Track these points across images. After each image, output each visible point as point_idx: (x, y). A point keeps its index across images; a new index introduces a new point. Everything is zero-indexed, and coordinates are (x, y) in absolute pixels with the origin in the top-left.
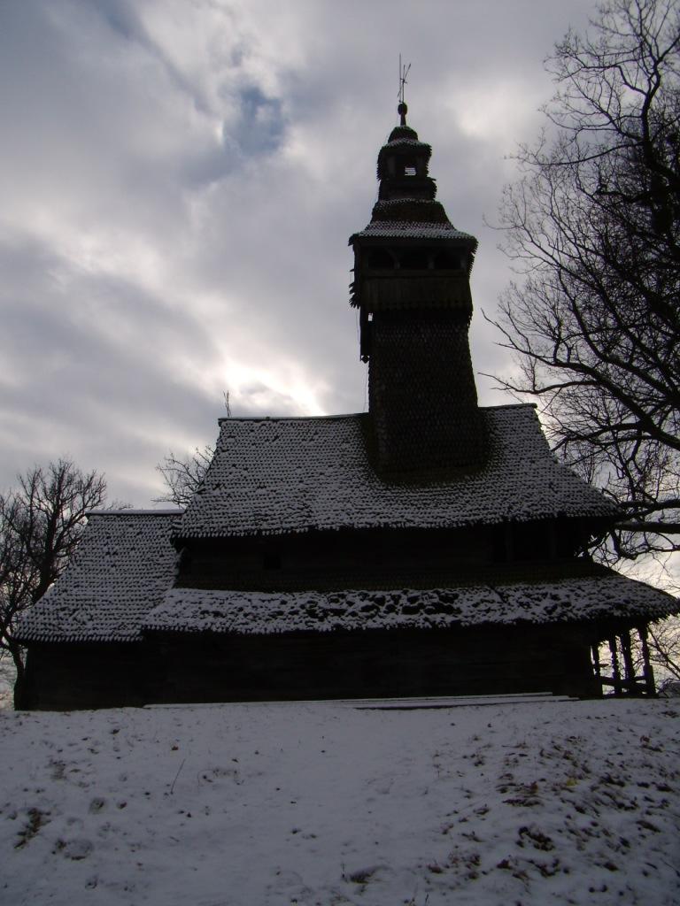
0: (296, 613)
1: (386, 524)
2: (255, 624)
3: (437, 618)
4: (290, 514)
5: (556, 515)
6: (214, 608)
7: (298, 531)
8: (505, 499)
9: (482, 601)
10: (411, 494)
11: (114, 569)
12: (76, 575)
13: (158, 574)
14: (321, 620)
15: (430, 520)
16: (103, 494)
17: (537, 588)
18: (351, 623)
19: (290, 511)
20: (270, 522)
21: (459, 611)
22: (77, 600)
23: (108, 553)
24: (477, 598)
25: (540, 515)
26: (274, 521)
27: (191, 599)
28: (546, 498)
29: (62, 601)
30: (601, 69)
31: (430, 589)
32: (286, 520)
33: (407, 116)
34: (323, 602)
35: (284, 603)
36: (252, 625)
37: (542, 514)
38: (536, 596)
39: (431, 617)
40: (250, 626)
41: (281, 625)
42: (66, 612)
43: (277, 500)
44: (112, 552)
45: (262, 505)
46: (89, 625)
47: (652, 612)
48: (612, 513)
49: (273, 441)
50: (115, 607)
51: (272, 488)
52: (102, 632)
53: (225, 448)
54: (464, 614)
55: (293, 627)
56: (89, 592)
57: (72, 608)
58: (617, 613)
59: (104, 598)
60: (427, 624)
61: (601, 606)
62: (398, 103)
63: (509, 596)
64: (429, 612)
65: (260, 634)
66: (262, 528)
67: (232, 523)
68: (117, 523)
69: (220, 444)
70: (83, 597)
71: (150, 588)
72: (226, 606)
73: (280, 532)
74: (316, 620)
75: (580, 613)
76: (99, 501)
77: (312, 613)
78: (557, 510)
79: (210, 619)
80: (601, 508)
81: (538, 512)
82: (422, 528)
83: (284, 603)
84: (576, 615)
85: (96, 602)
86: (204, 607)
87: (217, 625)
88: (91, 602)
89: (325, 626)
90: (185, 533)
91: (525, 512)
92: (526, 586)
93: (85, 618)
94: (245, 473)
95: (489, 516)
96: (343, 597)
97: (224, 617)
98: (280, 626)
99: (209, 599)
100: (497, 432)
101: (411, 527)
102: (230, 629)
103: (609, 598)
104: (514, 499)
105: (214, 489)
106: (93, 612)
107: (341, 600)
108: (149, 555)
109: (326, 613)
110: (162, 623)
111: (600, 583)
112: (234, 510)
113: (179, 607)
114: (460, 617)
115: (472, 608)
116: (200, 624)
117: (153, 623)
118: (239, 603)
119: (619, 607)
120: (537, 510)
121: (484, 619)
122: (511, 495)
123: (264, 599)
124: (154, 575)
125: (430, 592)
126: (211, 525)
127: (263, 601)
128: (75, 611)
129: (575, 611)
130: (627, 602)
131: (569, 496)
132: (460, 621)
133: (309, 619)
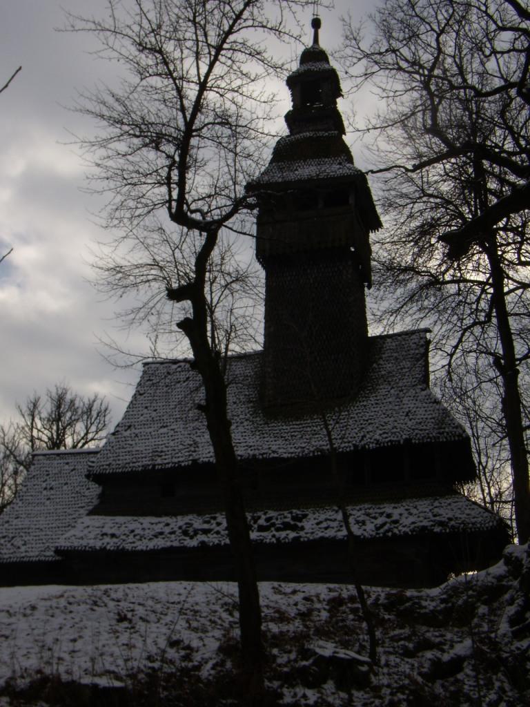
0: (173, 533)
1: (254, 455)
2: (140, 543)
3: (283, 534)
4: (180, 451)
5: (402, 442)
6: (110, 532)
7: (183, 464)
8: (363, 428)
9: (326, 520)
10: (284, 427)
11: (48, 502)
12: (17, 509)
13: (83, 505)
14: (192, 538)
15: (292, 450)
16: (107, 418)
17: (379, 508)
18: (214, 540)
19: (181, 447)
20: (163, 457)
21: (302, 528)
22: (16, 529)
23: (45, 489)
24: (323, 517)
25: (387, 442)
26: (167, 457)
27: (97, 524)
28: (398, 426)
29: (4, 531)
30: (369, 72)
31: (285, 510)
32: (177, 455)
33: (320, 31)
34: (198, 523)
35: (168, 525)
36: (138, 543)
37: (390, 441)
38: (373, 515)
39: (277, 534)
40: (135, 545)
41: (160, 543)
42: (7, 539)
43: (173, 438)
44: (48, 487)
45: (160, 443)
46: (23, 549)
47: (471, 529)
48: (457, 438)
49: (184, 382)
50: (44, 533)
51: (172, 427)
52: (32, 554)
53: (141, 392)
54: (305, 531)
55: (169, 544)
56: (27, 522)
57: (11, 535)
58: (437, 529)
59: (37, 527)
60: (274, 540)
61: (425, 523)
62: (312, 17)
63: (351, 515)
64: (278, 530)
65: (142, 550)
66: (156, 463)
67: (134, 460)
68: (56, 462)
69: (139, 388)
70: (20, 527)
71: (74, 516)
72: (123, 528)
73: (170, 466)
74: (187, 538)
75: (404, 529)
76: (105, 425)
77: (185, 533)
78: (404, 437)
79: (107, 539)
80: (448, 433)
81: (387, 440)
82: (283, 458)
83: (168, 525)
84: (400, 531)
85: (30, 530)
86: (105, 530)
87: (110, 544)
88: (27, 530)
89: (193, 543)
90: (97, 470)
91: (375, 440)
92: (370, 506)
93: (20, 543)
94: (154, 414)
95: (343, 445)
96: (215, 518)
97: (117, 538)
98: (159, 543)
99: (109, 523)
100: (381, 362)
101: (274, 458)
102: (121, 547)
103: (435, 516)
104: (370, 428)
105: (126, 430)
106: (26, 539)
107: (212, 521)
108: (77, 489)
109: (196, 532)
110: (69, 544)
111: (436, 504)
112: (138, 449)
113: (86, 531)
114: (302, 533)
115: (315, 526)
116: (98, 544)
117: (63, 544)
118: (132, 527)
119: (441, 524)
120: (386, 438)
121: (321, 534)
122: (369, 424)
123: (153, 522)
124: (80, 505)
125: (286, 513)
126: (118, 462)
127: (152, 524)
128: (13, 538)
129: (400, 528)
130: (450, 519)
131: (420, 423)
132: (300, 537)
133: (183, 537)
